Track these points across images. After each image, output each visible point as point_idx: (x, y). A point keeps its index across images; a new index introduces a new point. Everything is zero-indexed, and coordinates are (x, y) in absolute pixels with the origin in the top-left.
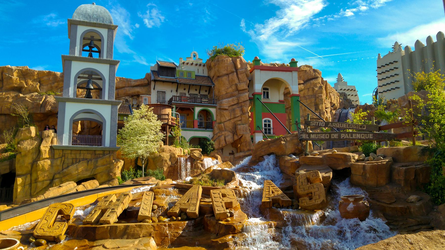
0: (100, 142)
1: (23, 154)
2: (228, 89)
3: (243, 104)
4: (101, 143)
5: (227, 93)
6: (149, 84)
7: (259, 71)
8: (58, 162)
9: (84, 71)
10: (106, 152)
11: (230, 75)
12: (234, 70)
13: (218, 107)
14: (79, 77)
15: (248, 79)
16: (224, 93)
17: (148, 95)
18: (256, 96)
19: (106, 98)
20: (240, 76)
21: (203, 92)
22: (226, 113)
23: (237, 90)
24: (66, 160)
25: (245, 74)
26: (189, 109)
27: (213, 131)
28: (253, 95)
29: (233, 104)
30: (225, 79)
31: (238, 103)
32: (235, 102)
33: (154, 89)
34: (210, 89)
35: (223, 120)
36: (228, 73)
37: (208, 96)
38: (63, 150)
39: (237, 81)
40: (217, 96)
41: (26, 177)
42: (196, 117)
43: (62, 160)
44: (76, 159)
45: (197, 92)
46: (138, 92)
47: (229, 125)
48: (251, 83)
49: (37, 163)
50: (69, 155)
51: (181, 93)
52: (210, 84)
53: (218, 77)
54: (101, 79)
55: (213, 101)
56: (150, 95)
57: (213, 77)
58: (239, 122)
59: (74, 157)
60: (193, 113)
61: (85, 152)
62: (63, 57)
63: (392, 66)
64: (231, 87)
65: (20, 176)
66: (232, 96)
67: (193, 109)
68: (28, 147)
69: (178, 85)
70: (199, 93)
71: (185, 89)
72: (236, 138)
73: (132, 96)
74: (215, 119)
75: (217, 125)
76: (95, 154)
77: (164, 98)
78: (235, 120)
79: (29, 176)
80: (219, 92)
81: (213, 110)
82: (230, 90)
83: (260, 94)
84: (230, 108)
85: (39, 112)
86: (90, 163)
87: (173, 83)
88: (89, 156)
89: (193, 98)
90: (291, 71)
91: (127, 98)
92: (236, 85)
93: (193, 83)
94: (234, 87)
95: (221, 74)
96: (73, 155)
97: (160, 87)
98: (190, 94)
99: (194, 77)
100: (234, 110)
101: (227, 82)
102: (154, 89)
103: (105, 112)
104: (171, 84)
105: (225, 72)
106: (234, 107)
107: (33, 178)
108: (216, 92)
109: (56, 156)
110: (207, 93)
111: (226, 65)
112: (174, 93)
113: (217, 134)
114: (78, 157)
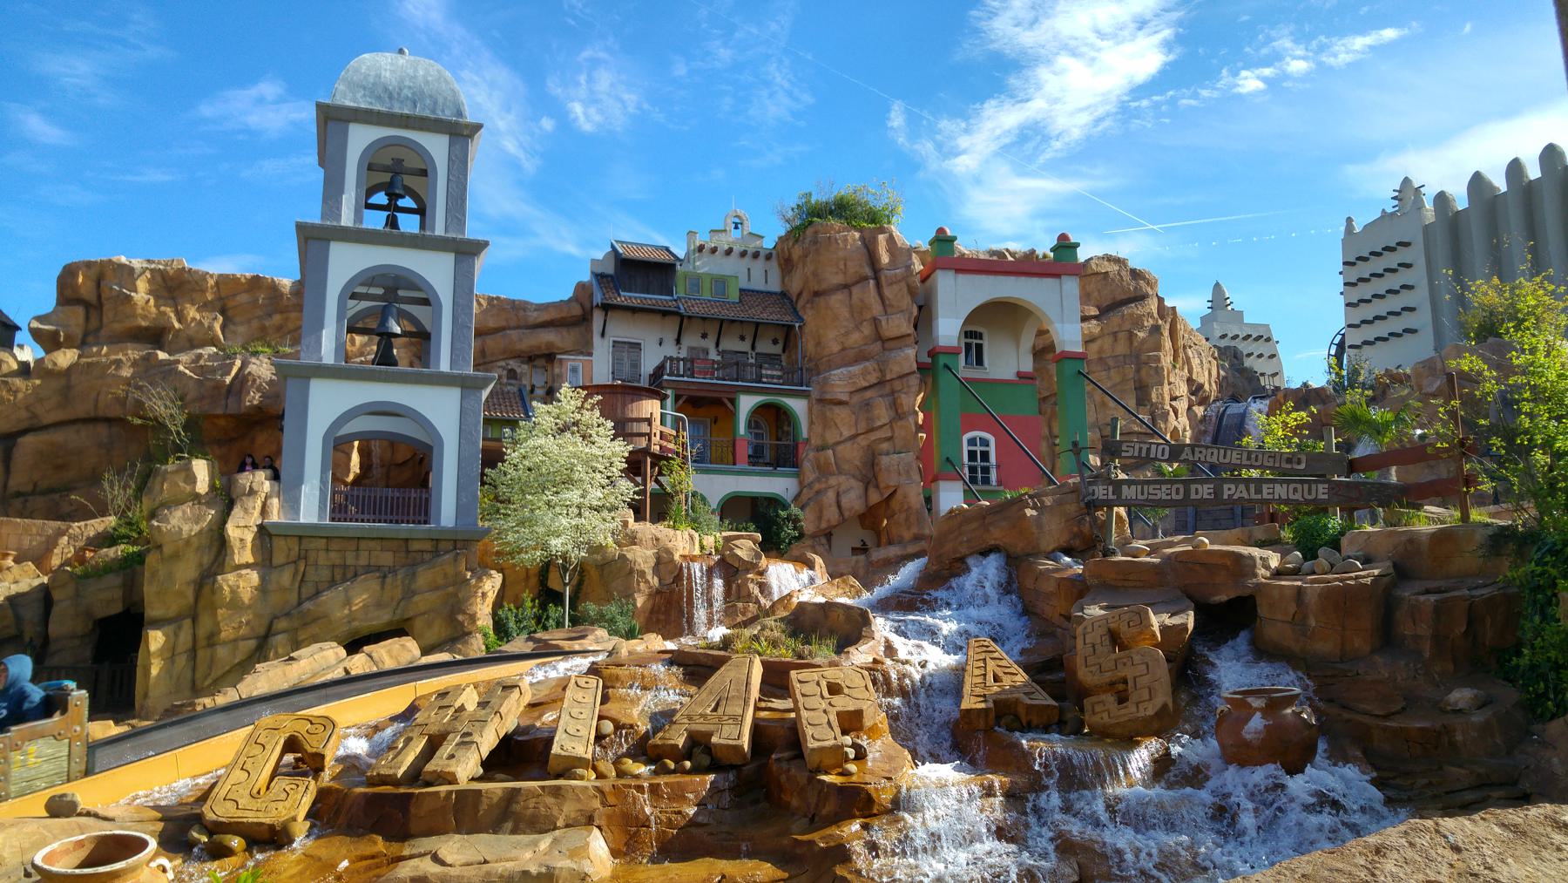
0: (423, 510)
1: (167, 550)
2: (847, 334)
3: (897, 385)
4: (426, 513)
5: (844, 349)
6: (584, 320)
7: (951, 274)
8: (286, 578)
9: (372, 277)
10: (442, 546)
11: (856, 290)
12: (868, 271)
13: (815, 395)
14: (354, 296)
15: (914, 301)
16: (836, 348)
17: (582, 353)
18: (942, 360)
19: (444, 366)
20: (887, 292)
21: (765, 347)
22: (841, 414)
23: (878, 337)
24: (311, 570)
25: (903, 284)
26: (718, 402)
27: (797, 475)
28: (933, 354)
29: (865, 384)
30: (836, 299)
31: (881, 383)
32: (873, 379)
33: (603, 335)
34: (788, 335)
35: (831, 437)
36: (849, 281)
37: (784, 358)
38: (300, 537)
39: (877, 309)
40: (810, 360)
41: (180, 628)
42: (742, 429)
43: (296, 571)
44: (345, 567)
45: (745, 346)
46: (550, 345)
47: (852, 454)
48: (924, 316)
49: (215, 581)
50: (322, 555)
51: (691, 349)
52: (787, 319)
53: (817, 294)
54: (425, 302)
55: (800, 376)
56: (590, 354)
57: (799, 295)
58: (885, 446)
59: (338, 562)
60: (732, 415)
61: (372, 544)
62: (301, 228)
63: (1391, 260)
64: (857, 327)
65: (157, 624)
66: (860, 357)
67: (733, 401)
68: (186, 528)
69: (682, 321)
70: (753, 348)
71: (704, 336)
72: (875, 498)
73: (530, 358)
74: (805, 433)
75: (811, 455)
76: (408, 552)
77: (636, 365)
78: (873, 436)
79: (187, 623)
80: (818, 344)
81: (798, 406)
82: (855, 338)
83: (953, 352)
84: (856, 399)
85: (219, 411)
86: (389, 580)
87: (665, 313)
88: (386, 559)
89: (734, 364)
90: (1057, 276)
91: (513, 364)
92: (875, 322)
93: (731, 315)
94: (867, 330)
95: (824, 286)
96: (333, 555)
97: (622, 330)
98: (722, 353)
99: (734, 296)
100: (867, 405)
101: (844, 313)
102: (603, 335)
103: (441, 411)
104: (658, 317)
105: (837, 279)
106: (868, 394)
107: (202, 632)
108: (808, 344)
109: (279, 558)
110: (777, 349)
111: (841, 254)
112: (670, 350)
113: (810, 485)
114: (350, 561)
